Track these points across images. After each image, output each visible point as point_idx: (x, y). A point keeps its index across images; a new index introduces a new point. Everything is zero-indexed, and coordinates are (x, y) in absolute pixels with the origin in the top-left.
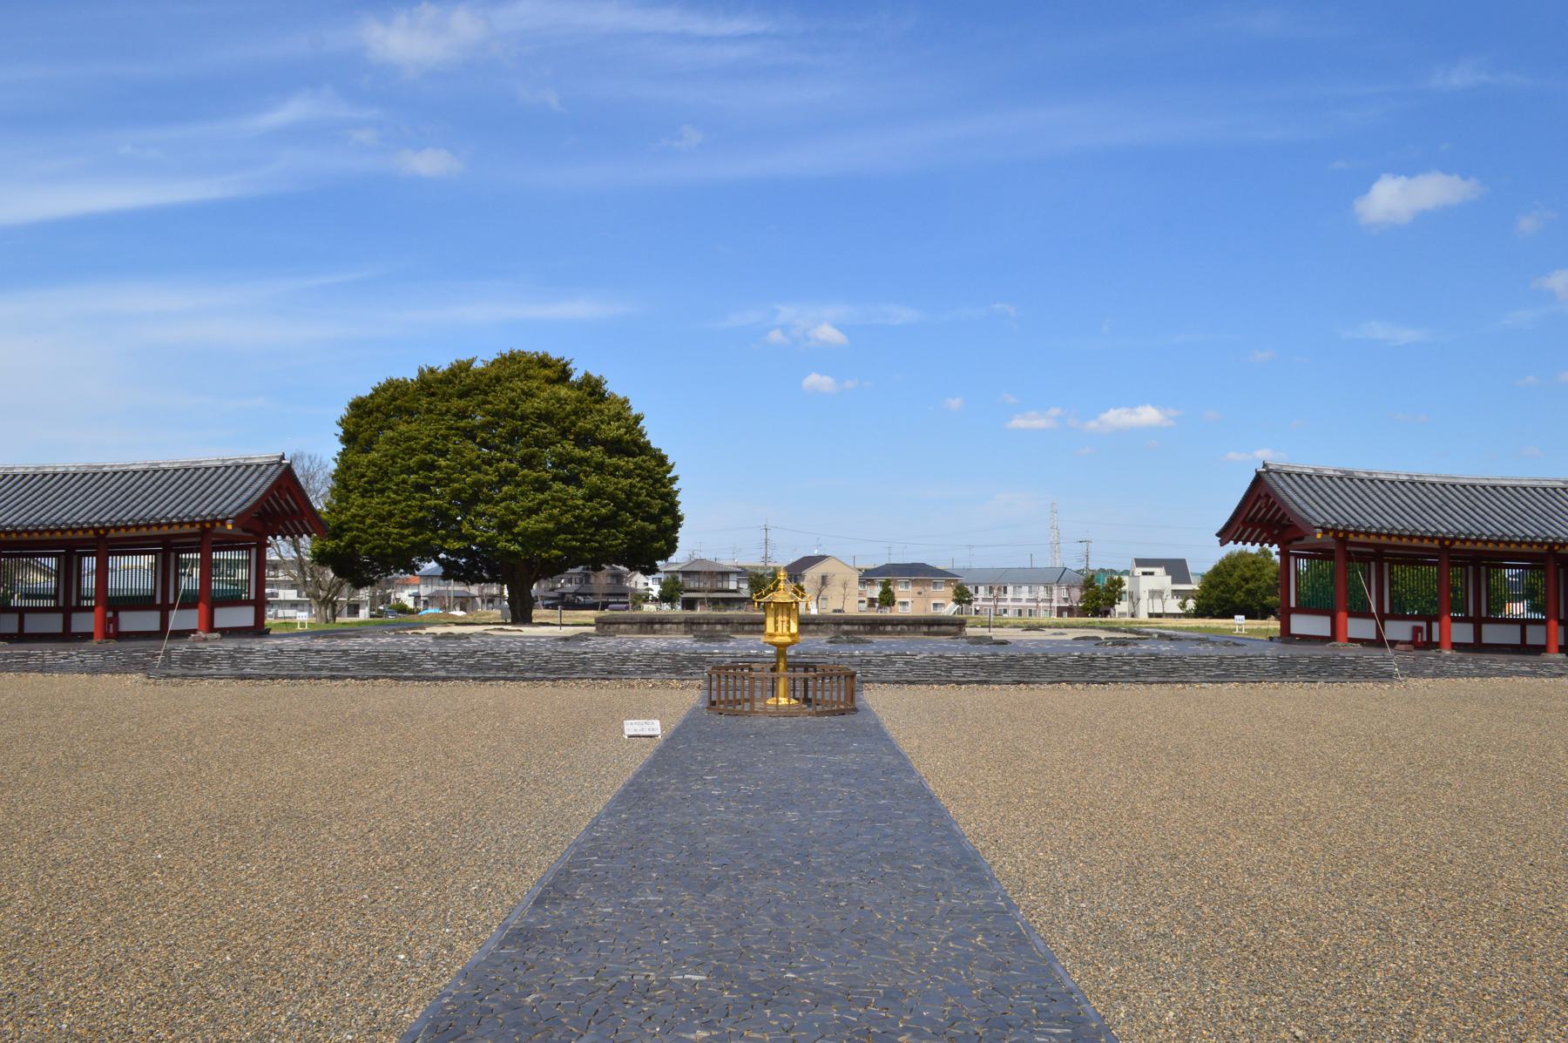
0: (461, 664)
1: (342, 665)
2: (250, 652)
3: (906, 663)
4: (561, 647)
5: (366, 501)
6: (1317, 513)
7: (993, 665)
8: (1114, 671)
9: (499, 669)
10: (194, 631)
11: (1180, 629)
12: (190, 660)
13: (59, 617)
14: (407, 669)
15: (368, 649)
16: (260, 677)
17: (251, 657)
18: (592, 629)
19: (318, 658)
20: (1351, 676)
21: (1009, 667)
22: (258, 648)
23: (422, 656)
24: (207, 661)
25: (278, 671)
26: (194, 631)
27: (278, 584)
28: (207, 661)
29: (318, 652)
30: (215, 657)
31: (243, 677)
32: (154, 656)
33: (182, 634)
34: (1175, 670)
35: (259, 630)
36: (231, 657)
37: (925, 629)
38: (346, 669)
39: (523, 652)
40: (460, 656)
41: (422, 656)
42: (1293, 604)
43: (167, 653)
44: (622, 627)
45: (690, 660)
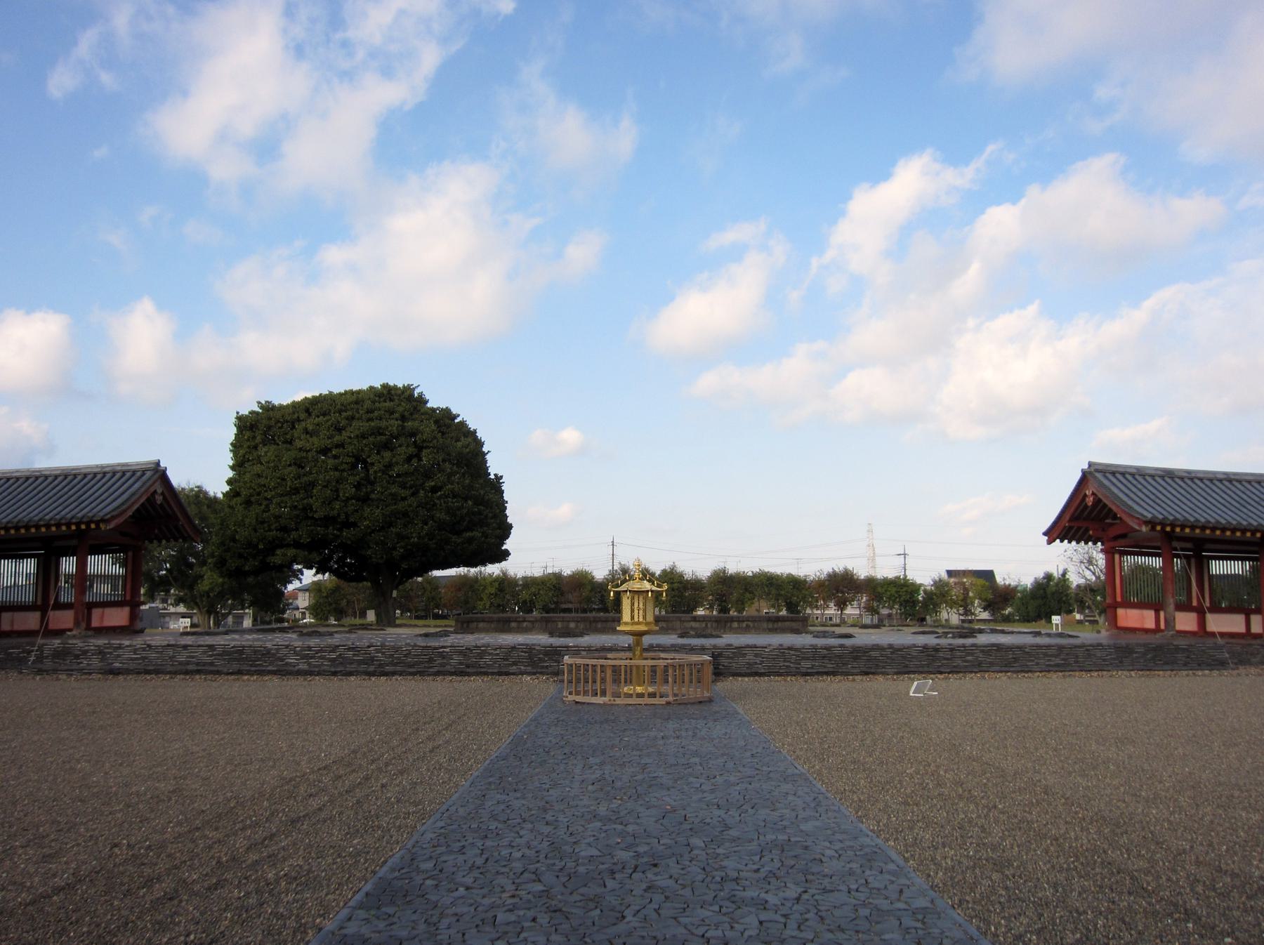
0: (323, 658)
1: (208, 660)
2: (120, 647)
3: (756, 655)
4: (421, 642)
5: (763, 895)
6: (1142, 508)
7: (839, 657)
8: (959, 662)
9: (360, 662)
10: (70, 630)
11: (410, 626)
12: (60, 654)
13: (37, 615)
14: (271, 663)
15: (233, 644)
16: (127, 672)
17: (120, 652)
18: (1162, 614)
19: (185, 653)
20: (1185, 665)
21: (856, 658)
22: (127, 643)
23: (285, 651)
24: (77, 657)
25: (148, 668)
26: (70, 630)
27: (112, 579)
28: (77, 657)
29: (185, 647)
30: (87, 651)
31: (116, 672)
32: (29, 652)
33: (59, 633)
34: (1016, 660)
35: (131, 629)
36: (101, 652)
37: (765, 625)
38: (212, 664)
39: (383, 645)
40: (321, 651)
41: (285, 651)
42: (1119, 599)
43: (41, 648)
44: (481, 625)
45: (547, 653)
